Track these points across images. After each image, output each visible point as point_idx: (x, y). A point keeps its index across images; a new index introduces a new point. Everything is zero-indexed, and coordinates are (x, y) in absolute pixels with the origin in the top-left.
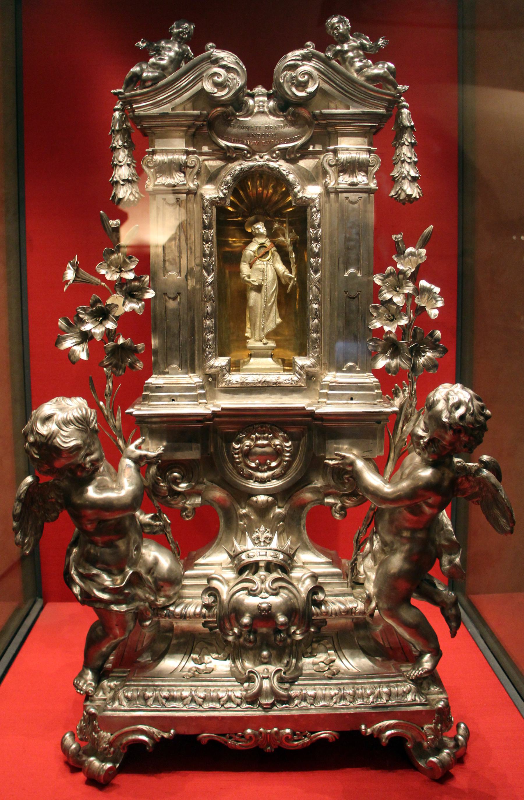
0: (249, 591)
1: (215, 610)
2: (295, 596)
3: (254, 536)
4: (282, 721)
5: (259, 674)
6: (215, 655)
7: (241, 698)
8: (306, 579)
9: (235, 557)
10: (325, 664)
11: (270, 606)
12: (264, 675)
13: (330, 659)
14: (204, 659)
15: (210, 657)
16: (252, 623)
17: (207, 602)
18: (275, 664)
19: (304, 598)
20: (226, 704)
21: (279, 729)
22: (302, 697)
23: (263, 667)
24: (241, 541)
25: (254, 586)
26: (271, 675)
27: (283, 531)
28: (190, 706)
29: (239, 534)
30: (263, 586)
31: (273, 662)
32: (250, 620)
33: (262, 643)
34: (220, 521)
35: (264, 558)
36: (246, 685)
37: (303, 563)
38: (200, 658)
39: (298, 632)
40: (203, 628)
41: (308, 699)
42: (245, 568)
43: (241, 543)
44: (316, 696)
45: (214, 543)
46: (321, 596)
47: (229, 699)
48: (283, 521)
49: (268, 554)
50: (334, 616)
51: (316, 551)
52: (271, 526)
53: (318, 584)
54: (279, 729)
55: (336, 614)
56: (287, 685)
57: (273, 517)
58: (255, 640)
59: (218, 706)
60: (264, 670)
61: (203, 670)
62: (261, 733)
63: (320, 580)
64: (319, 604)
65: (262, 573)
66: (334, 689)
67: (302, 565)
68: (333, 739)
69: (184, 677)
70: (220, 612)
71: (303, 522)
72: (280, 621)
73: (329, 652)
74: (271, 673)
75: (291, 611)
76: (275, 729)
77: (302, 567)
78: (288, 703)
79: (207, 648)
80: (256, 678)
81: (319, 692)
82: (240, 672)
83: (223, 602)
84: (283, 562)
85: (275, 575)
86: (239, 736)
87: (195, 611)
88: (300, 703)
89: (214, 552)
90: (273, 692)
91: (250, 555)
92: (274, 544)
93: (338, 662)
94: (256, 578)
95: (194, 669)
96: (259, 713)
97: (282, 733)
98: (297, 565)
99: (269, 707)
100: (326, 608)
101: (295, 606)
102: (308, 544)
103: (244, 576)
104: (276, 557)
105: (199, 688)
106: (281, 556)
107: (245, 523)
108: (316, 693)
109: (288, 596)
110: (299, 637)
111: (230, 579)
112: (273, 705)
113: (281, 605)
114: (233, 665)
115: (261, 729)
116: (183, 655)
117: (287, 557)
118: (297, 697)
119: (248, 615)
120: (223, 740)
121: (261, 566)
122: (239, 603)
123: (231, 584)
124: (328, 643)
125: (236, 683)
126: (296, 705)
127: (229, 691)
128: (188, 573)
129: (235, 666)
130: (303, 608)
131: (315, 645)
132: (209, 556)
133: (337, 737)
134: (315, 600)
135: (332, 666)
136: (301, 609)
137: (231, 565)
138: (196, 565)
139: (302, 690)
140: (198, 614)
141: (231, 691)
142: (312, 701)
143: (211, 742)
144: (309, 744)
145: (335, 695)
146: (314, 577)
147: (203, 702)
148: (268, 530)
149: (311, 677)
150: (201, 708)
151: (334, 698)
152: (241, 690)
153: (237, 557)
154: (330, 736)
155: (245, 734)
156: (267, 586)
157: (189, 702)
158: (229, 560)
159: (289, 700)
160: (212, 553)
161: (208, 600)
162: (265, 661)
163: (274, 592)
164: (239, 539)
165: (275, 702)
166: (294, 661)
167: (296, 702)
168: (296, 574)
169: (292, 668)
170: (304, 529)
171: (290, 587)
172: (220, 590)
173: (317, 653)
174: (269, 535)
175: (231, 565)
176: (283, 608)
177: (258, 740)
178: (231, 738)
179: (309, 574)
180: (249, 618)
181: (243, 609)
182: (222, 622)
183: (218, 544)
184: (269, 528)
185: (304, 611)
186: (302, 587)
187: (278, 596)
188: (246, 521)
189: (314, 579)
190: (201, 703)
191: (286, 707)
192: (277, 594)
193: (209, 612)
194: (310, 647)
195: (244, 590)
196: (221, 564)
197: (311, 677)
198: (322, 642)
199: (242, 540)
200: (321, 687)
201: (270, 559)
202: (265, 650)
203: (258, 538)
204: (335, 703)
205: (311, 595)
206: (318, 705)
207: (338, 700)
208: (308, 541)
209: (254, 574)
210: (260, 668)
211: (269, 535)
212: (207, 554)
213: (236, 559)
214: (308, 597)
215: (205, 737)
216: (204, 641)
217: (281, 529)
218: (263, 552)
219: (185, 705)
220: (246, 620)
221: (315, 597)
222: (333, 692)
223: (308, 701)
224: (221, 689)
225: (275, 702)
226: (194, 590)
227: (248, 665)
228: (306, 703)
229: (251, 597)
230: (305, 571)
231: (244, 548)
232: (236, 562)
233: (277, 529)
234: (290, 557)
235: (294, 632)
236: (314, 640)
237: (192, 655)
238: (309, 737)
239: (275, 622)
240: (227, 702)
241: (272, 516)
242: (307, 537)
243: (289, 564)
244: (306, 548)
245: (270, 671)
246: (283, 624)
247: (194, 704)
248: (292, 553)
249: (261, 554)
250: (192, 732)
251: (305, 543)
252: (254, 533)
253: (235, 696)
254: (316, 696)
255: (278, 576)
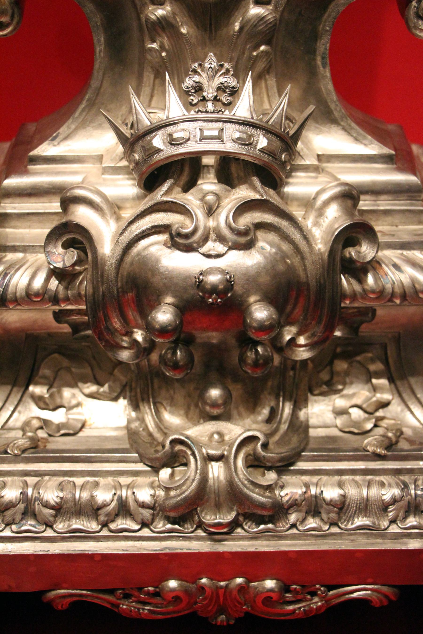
0: (172, 237)
1: (84, 284)
2: (297, 249)
3: (188, 83)
4: (254, 564)
5: (200, 448)
6: (93, 388)
7: (152, 508)
8: (327, 203)
9: (134, 141)
10: (365, 411)
11: (229, 281)
12: (212, 452)
13: (377, 401)
14: (61, 397)
15: (76, 391)
16: (181, 322)
17: (60, 265)
18: (240, 415)
19: (321, 254)
20: (113, 521)
21: (249, 580)
22: (309, 506)
23: (210, 427)
24: (152, 96)
25: (188, 222)
26: (230, 451)
27: (268, 70)
28: (24, 528)
29: (149, 76)
30: (211, 223)
31: (235, 413)
32: (176, 315)
33: (207, 366)
34: (95, 39)
35: (216, 146)
36: (165, 473)
37: (319, 157)
38: (52, 396)
39: (302, 340)
40: (57, 325)
41: (322, 511)
42: (163, 173)
43: (153, 103)
44: (344, 503)
45: (80, 103)
46: (366, 251)
47: (123, 509)
48: (268, 43)
49: (226, 135)
50: (398, 301)
51: (353, 125)
52: (235, 55)
53: (357, 218)
54: (249, 580)
55: (404, 296)
56: (271, 476)
57: (242, 28)
58: (190, 359)
59: (94, 526)
60: (211, 436)
61: (59, 427)
62: (202, 588)
63: (365, 204)
64: (358, 270)
65: (209, 184)
66: (390, 486)
67: (316, 163)
68: (381, 601)
69: (6, 452)
70: (95, 289)
71: (323, 45)
72: (256, 321)
73: (374, 381)
74: (231, 446)
75: (286, 290)
76: (239, 580)
77: (316, 169)
78: (271, 519)
79: (68, 369)
80: (191, 458)
81: (352, 492)
82: (150, 435)
83: (104, 264)
84: (266, 158)
85: (244, 193)
86: (148, 593)
87: (29, 284)
88: (304, 520)
89: (83, 125)
90: (233, 495)
91: (176, 136)
92: (244, 107)
93: (396, 407)
94: (191, 200)
95: (36, 423)
96: (199, 545)
97: (256, 588)
98: (303, 163)
99: (225, 530)
100: (376, 279)
101: (298, 276)
102: (333, 106)
103: (159, 195)
104: (247, 142)
105: (47, 478)
106: (263, 142)
107: (163, 48)
108: (344, 496)
109: (279, 249)
110: (303, 354)
111: (125, 199)
112: (235, 524)
113: (258, 274)
114: (133, 414)
115: (204, 581)
116: (9, 388)
117: (277, 143)
118: (295, 504)
119: (169, 299)
120: (108, 602)
121: (207, 166)
122: (148, 266)
123: (128, 214)
124: (373, 361)
125: (140, 467)
126: (294, 526)
127: (121, 486)
128: (11, 182)
129: (138, 419)
130: (318, 282)
131: (341, 366)
132: (66, 138)
133: (393, 598)
134: (351, 260)
135: (382, 418)
136: (313, 283)
137: (124, 163)
138: (36, 160)
139: (307, 486)
140: (37, 295)
141: (128, 487)
142: (333, 516)
143: (79, 606)
144: (323, 610)
145: (394, 501)
146: (350, 196)
147: (55, 516)
148: (227, 65)
149: (331, 449)
150: (49, 533)
151: (391, 508)
152: (152, 486)
153: (141, 143)
154: (375, 596)
155: (162, 589)
156: (223, 224)
157: (18, 517)
158: (120, 149)
159: (277, 512)
160: (76, 129)
161: (62, 257)
162: (215, 412)
163: (243, 240)
164: (146, 90)
165: (241, 519)
166: (288, 409)
167: (293, 518)
168: (299, 186)
169: (284, 427)
170: (324, 67)
171: (284, 224)
172: (93, 232)
173: (344, 384)
174: (232, 82)
175: (124, 163)
176: (264, 279)
177: (196, 603)
178: (127, 596)
179: (337, 190)
180: (171, 309)
181: (156, 280)
182: (101, 314)
183: (92, 104)
184: (230, 61)
185: (321, 288)
186: (316, 224)
187: (253, 251)
188: (166, 41)
189: (350, 203)
190: (52, 519)
191: (268, 531)
192: (248, 246)
193: (66, 288)
194: (328, 368)
195: (159, 233)
196: (100, 158)
197: (331, 449)
198: (358, 358)
199: (157, 93)
200: (358, 478)
201: (230, 147)
202: (213, 385)
203: (199, 89)
204: (393, 521)
205: (340, 247)
206: (350, 526)
207: (401, 515)
208: (335, 98)
209: (186, 189)
210: (200, 432)
211: (232, 82)
212: (63, 130)
213: (138, 147)
214: (332, 252)
215: (64, 596)
216: (60, 353)
217: (261, 66)
218: (211, 129)
219: (8, 524)
220: (164, 316)
221: (351, 252)
222: (388, 494)
223: (324, 516)
224: (102, 481)
225: (241, 519)
226: (29, 227)
227: (172, 419)
228: (317, 520)
229: (178, 253)
230: (323, 179)
231: (160, 116)
232: (137, 157)
233: (252, 63)
234: (287, 142)
235: (293, 341)
236: (339, 350)
237: (31, 388)
238: (322, 598)
239: (244, 321)
240: (117, 515)
241: (237, 26)
242: (331, 86)
243: (284, 164)
244: (326, 117)
245: (227, 438)
246: (262, 328)
247: (33, 522)
248: (292, 133)
249: (206, 133)
250: (29, 586)
251: (327, 106)
252: (187, 75)
253: (136, 501)
254: (344, 503)
255: (253, 195)
